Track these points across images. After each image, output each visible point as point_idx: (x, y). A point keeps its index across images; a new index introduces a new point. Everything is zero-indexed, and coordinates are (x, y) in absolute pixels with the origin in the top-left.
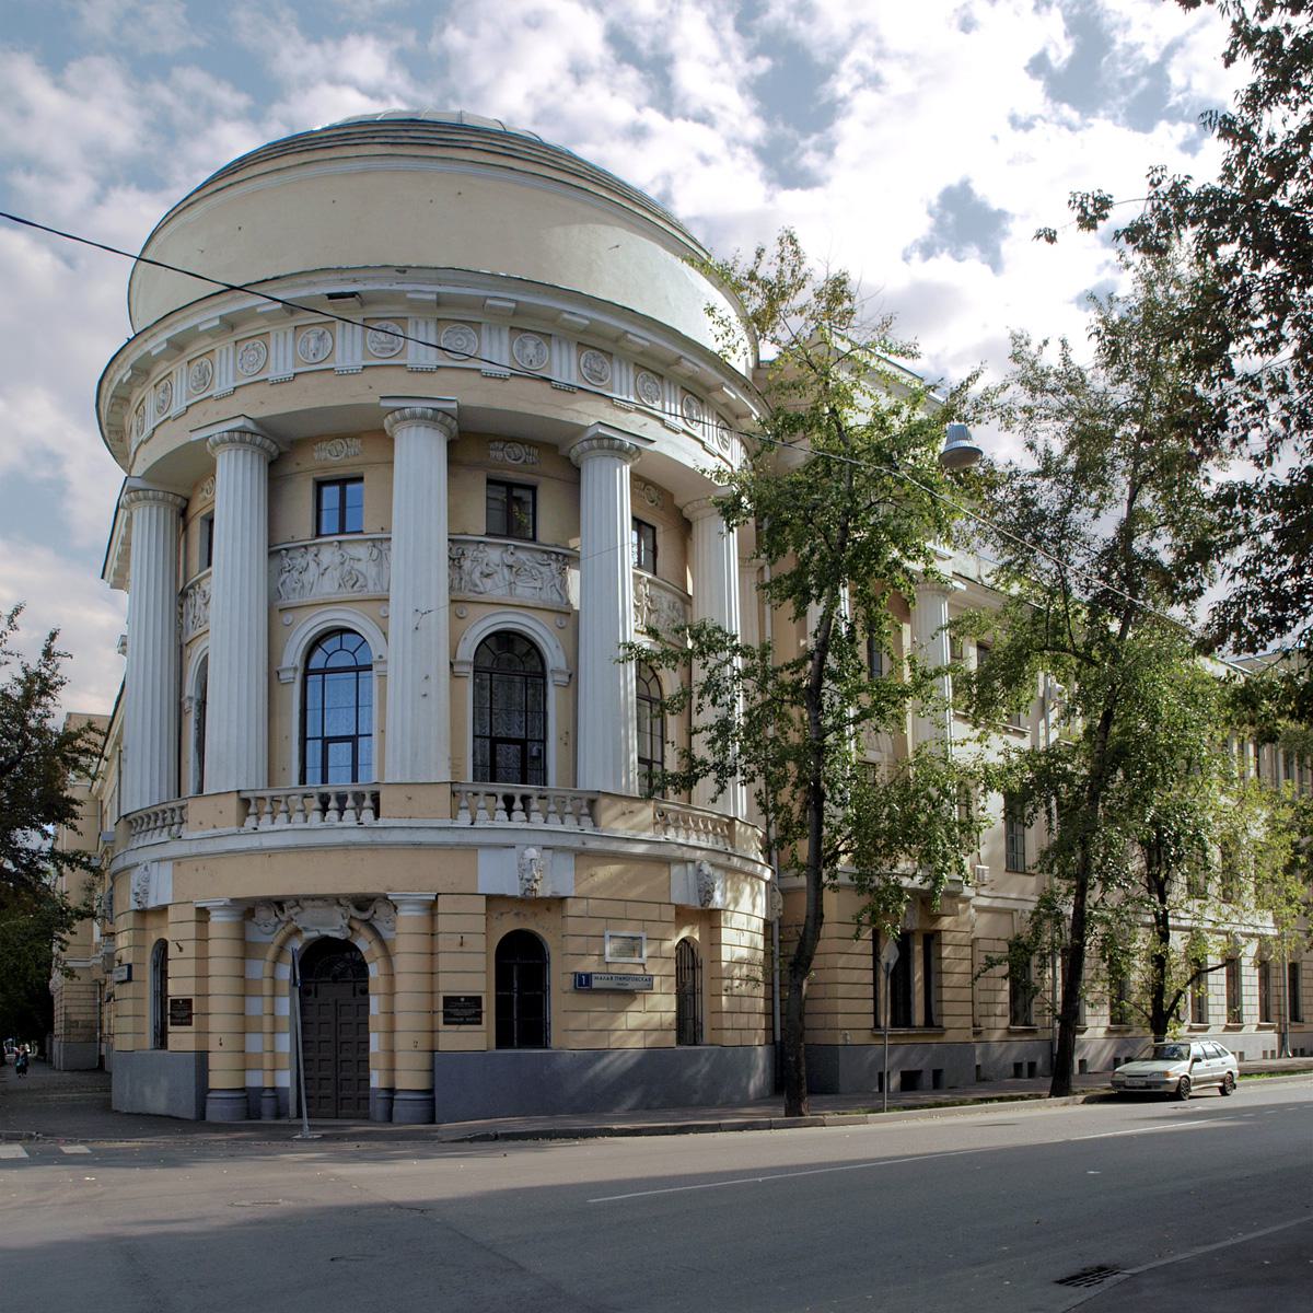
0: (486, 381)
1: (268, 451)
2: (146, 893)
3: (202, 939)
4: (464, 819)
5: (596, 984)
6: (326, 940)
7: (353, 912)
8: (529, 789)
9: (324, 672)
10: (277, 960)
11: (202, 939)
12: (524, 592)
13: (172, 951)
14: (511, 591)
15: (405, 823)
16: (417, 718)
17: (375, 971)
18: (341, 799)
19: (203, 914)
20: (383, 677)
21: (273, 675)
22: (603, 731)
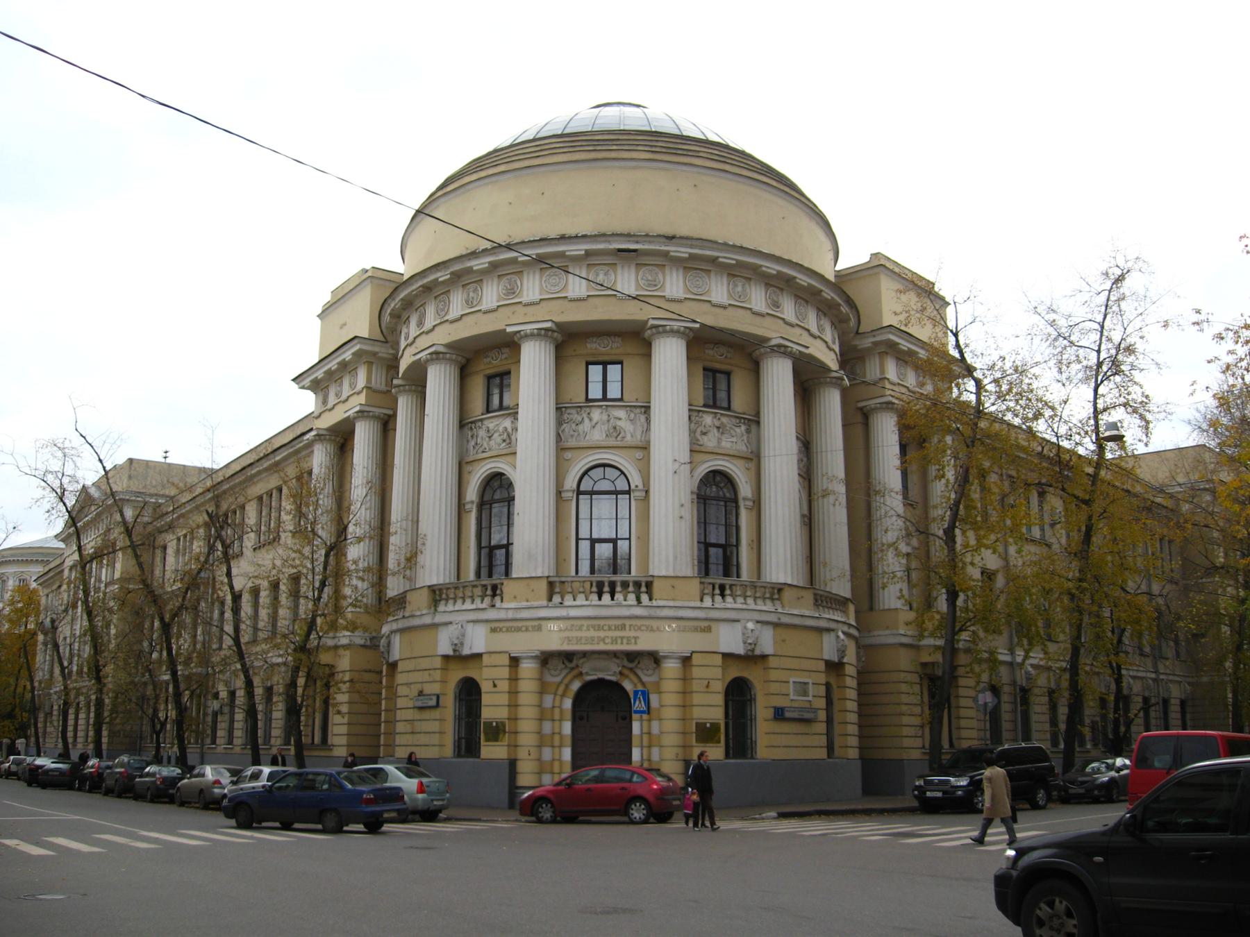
0: (714, 309)
1: (555, 339)
2: (462, 644)
3: (514, 679)
4: (708, 602)
5: (787, 715)
6: (601, 682)
7: (626, 662)
8: (727, 581)
9: (592, 493)
10: (563, 695)
11: (514, 679)
12: (727, 444)
13: (485, 686)
15: (671, 603)
16: (669, 541)
19: (515, 661)
21: (559, 493)
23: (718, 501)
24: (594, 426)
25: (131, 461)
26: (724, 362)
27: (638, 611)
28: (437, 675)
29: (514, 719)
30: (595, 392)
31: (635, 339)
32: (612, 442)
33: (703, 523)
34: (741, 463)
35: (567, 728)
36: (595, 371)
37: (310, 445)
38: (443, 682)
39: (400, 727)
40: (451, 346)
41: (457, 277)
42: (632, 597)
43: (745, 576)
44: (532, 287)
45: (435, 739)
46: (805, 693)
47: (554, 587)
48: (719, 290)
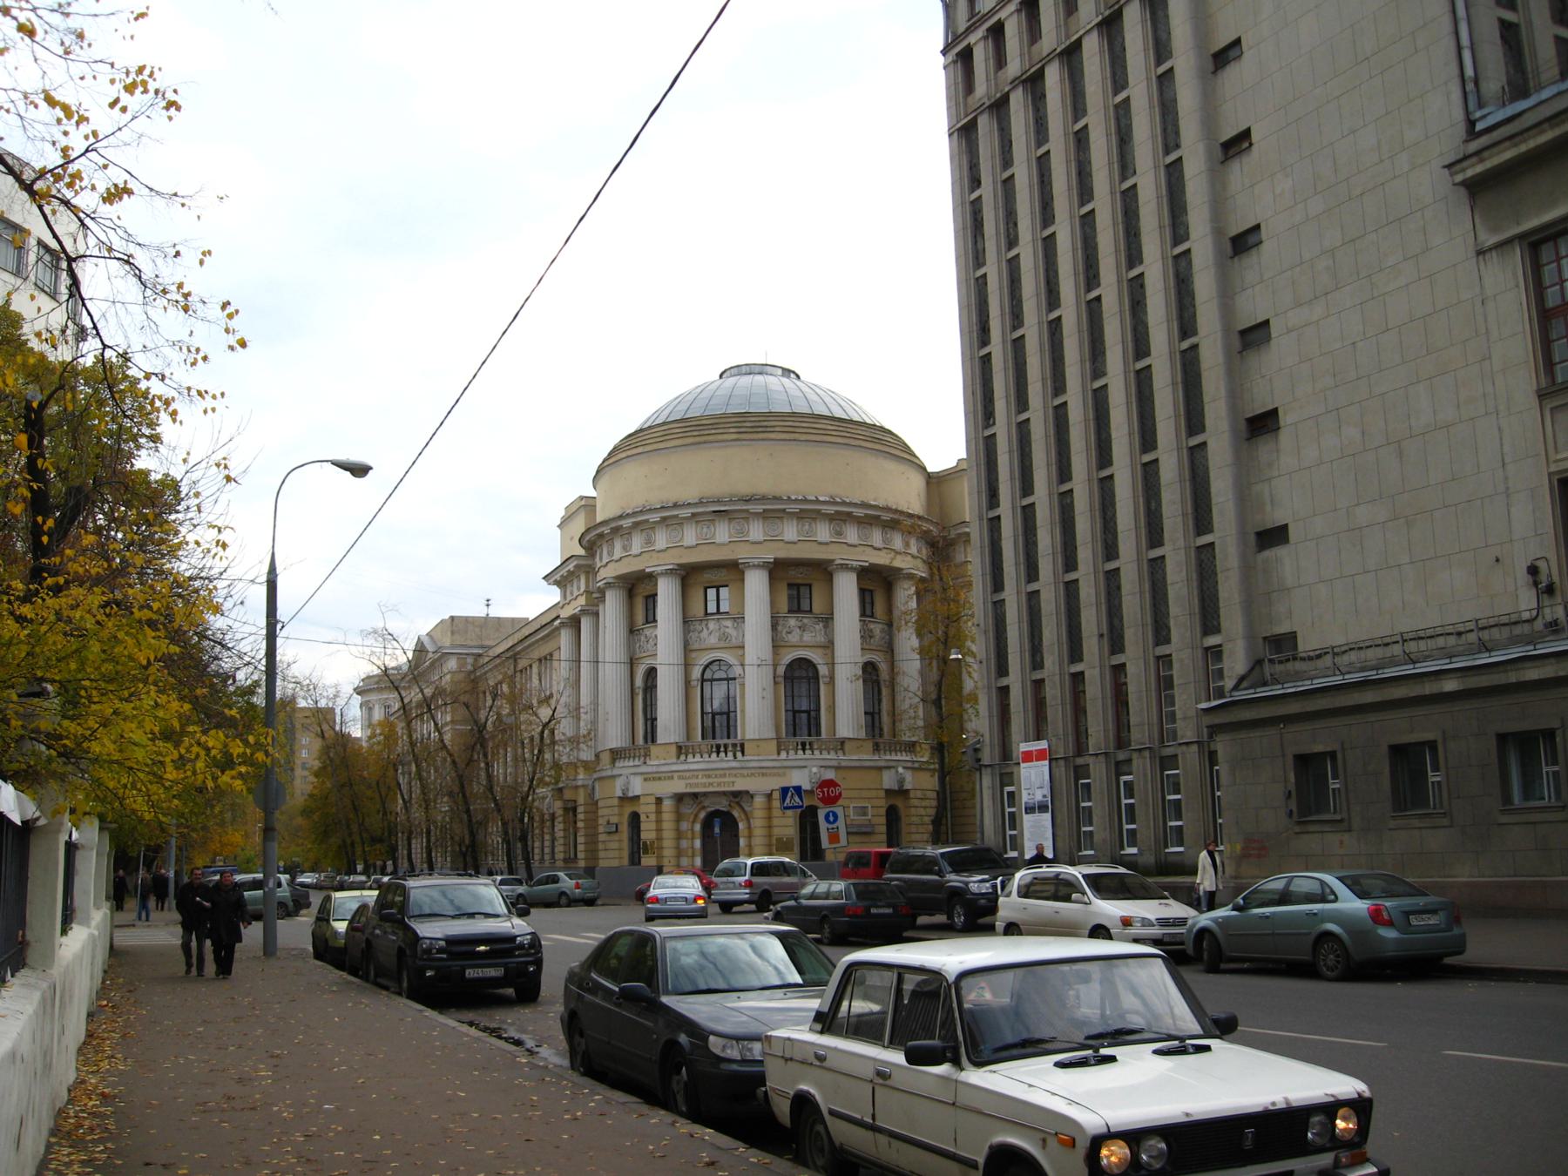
3: (659, 812)
4: (783, 755)
8: (813, 738)
9: (712, 680)
11: (659, 812)
12: (807, 637)
13: (643, 818)
14: (802, 639)
16: (757, 710)
17: (741, 826)
18: (726, 746)
19: (659, 801)
20: (743, 685)
21: (687, 682)
22: (845, 708)
23: (800, 681)
24: (709, 635)
25: (452, 618)
26: (799, 583)
27: (734, 764)
28: (616, 810)
29: (659, 839)
30: (712, 608)
31: (732, 571)
32: (722, 644)
33: (791, 696)
34: (820, 651)
35: (698, 843)
36: (712, 593)
37: (557, 629)
38: (620, 815)
39: (601, 846)
40: (619, 578)
41: (616, 530)
42: (730, 754)
43: (824, 735)
44: (661, 539)
45: (616, 854)
46: (865, 814)
47: (681, 750)
48: (790, 531)
